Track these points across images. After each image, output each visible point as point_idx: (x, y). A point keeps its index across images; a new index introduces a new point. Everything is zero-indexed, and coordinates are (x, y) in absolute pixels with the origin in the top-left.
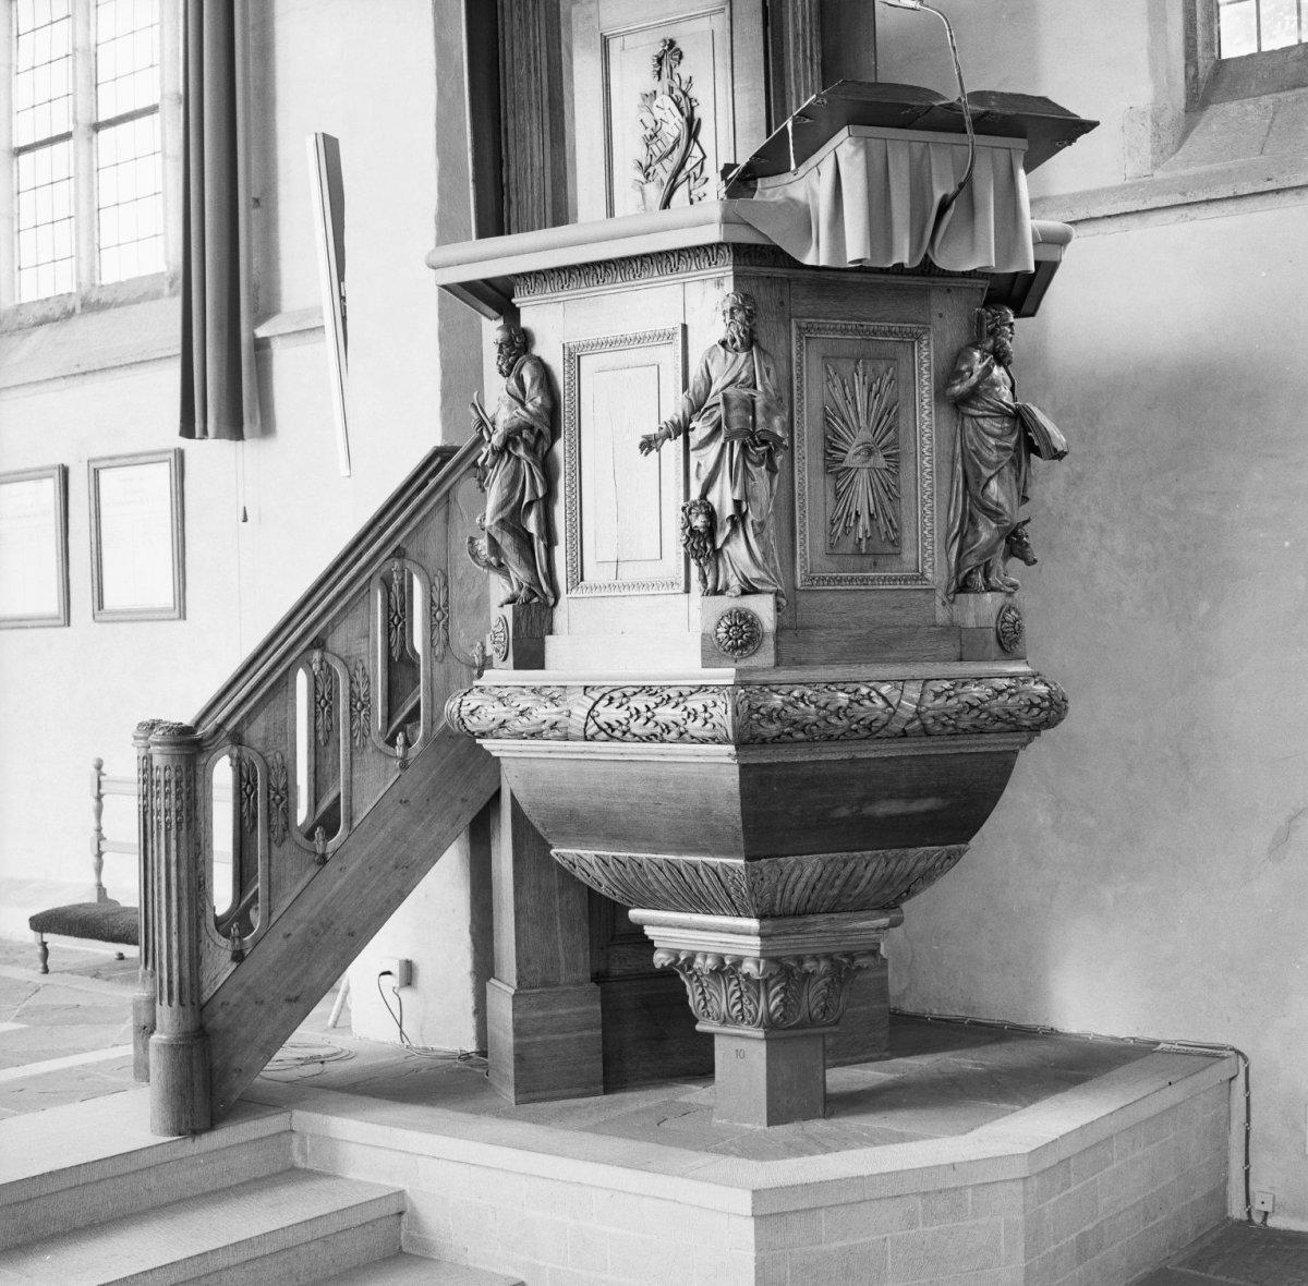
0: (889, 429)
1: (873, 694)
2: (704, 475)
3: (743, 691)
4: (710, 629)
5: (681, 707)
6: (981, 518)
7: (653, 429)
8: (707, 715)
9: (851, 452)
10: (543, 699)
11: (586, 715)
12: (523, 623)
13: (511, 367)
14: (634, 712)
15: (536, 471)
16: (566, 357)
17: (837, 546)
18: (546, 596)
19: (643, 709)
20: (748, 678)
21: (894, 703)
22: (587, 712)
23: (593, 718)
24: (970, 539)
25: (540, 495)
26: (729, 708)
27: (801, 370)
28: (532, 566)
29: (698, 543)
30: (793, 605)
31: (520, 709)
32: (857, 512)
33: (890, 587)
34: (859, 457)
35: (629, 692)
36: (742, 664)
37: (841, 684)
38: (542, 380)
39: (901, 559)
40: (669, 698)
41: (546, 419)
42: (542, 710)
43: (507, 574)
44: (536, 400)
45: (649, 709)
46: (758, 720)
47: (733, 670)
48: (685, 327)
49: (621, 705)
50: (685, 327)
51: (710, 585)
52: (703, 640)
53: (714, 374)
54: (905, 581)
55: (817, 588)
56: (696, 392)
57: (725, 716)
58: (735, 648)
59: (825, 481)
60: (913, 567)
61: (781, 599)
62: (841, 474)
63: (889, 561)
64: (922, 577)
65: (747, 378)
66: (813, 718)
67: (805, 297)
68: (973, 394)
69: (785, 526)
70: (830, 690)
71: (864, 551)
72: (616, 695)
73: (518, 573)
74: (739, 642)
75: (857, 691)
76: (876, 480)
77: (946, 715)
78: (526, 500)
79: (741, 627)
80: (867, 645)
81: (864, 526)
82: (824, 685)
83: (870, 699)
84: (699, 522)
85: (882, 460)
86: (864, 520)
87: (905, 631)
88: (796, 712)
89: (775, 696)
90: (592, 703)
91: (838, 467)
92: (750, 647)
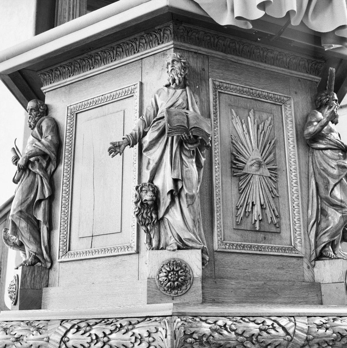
0: (270, 153)
1: (276, 325)
2: (152, 165)
3: (179, 320)
4: (154, 274)
5: (130, 333)
6: (330, 211)
7: (118, 138)
8: (151, 339)
9: (249, 164)
10: (32, 329)
11: (59, 340)
12: (28, 279)
13: (35, 122)
14: (94, 337)
15: (45, 182)
16: (69, 114)
17: (241, 223)
18: (45, 260)
19: (101, 335)
20: (182, 311)
21: (291, 331)
22: (61, 337)
23: (65, 343)
24: (323, 225)
25: (47, 195)
26: (169, 333)
27: (216, 109)
28: (38, 241)
29: (147, 213)
30: (213, 261)
31: (16, 336)
32: (253, 203)
33: (276, 254)
34: (253, 168)
35: (92, 322)
36: (178, 301)
37: (252, 318)
38: (53, 127)
39: (281, 237)
40: (121, 326)
41: (53, 149)
42: (31, 337)
43: (24, 250)
44: (48, 138)
45: (105, 335)
46: (191, 343)
47: (171, 304)
48: (141, 84)
49: (85, 332)
50: (141, 84)
51: (154, 243)
52: (149, 282)
53: (159, 104)
54: (285, 250)
55: (229, 251)
56: (148, 116)
57: (165, 340)
58: (172, 288)
59: (232, 181)
60: (289, 242)
61: (205, 255)
62: (242, 177)
63: (273, 237)
64: (294, 249)
65: (182, 103)
66: (233, 343)
67: (218, 69)
68: (318, 136)
69: (207, 207)
70: (244, 321)
71: (258, 229)
72: (83, 325)
73: (30, 248)
74: (176, 283)
75: (263, 322)
76: (264, 183)
77: (326, 342)
78: (37, 199)
79: (177, 272)
80: (263, 292)
81: (257, 212)
82: (240, 318)
83: (274, 328)
84: (147, 196)
85: (268, 171)
86: (257, 208)
87: (287, 284)
88: (221, 337)
89: (204, 324)
90: (64, 331)
91: (240, 173)
92: (184, 288)
